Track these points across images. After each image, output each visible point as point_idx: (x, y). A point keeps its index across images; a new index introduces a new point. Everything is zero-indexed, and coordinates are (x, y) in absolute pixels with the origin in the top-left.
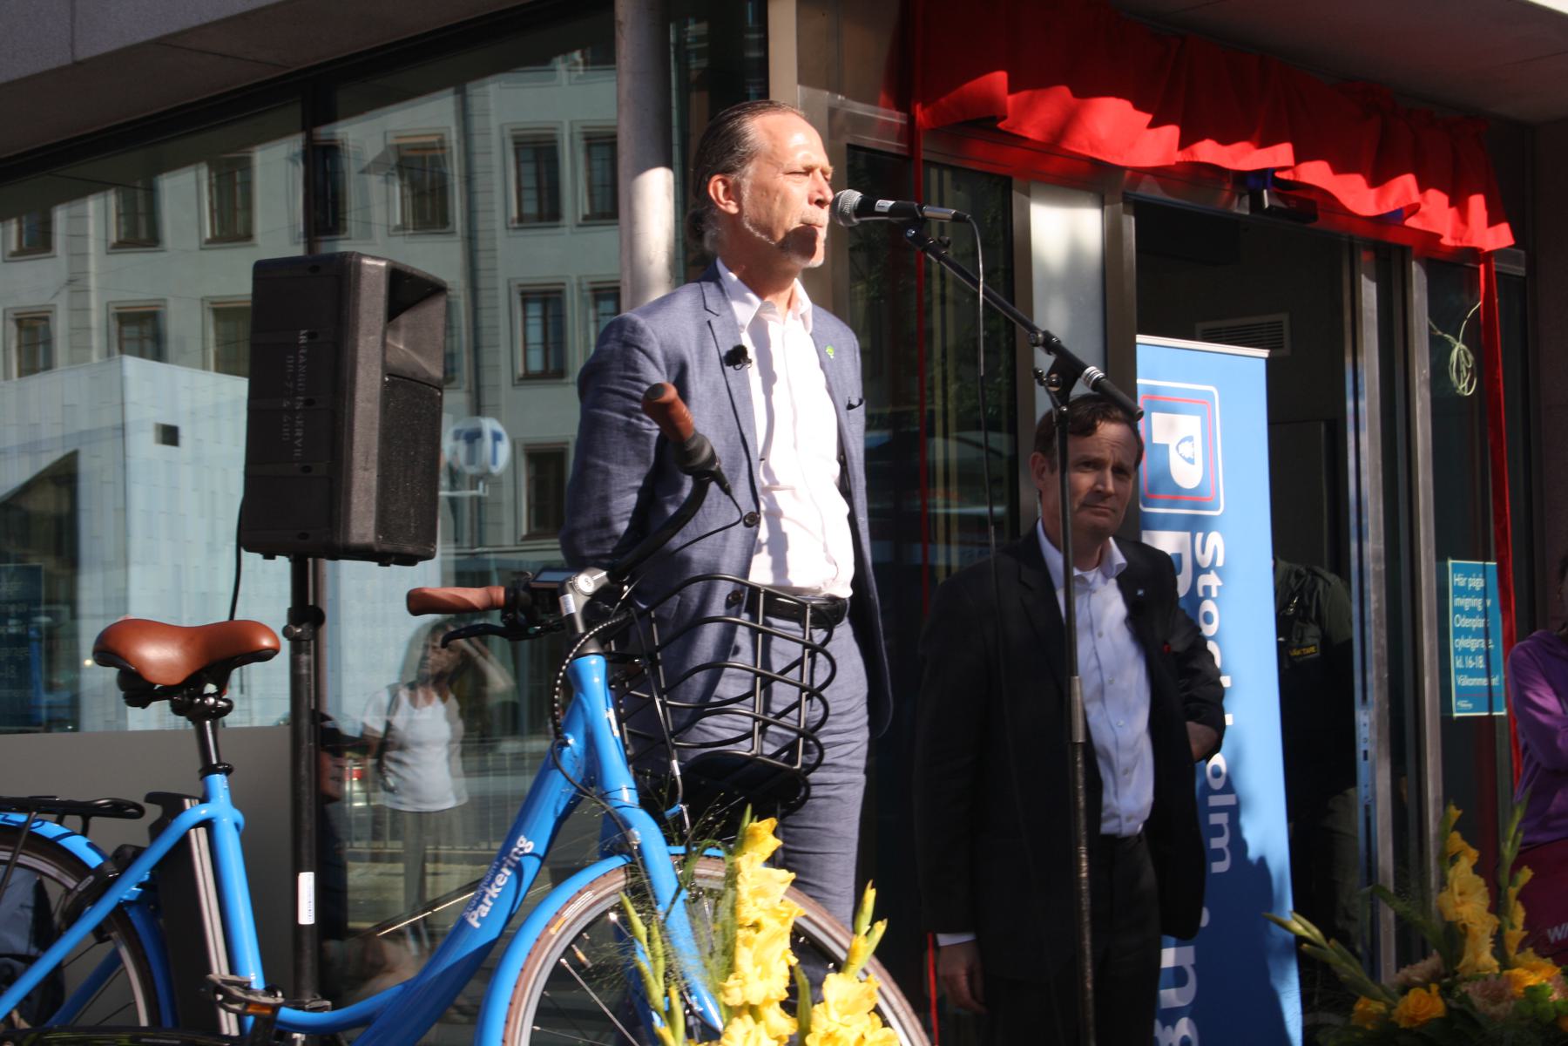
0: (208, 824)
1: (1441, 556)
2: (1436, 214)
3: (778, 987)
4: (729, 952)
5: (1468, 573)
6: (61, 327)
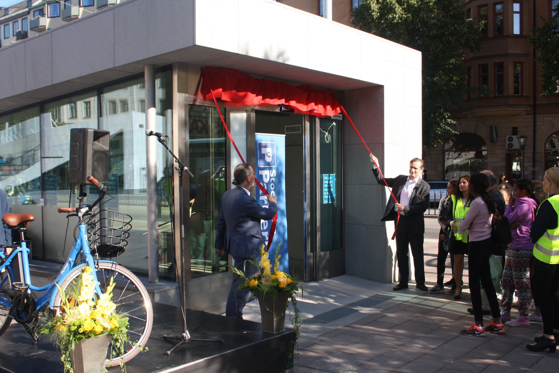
0: (21, 252)
1: (322, 172)
2: (319, 109)
3: (92, 295)
4: (80, 291)
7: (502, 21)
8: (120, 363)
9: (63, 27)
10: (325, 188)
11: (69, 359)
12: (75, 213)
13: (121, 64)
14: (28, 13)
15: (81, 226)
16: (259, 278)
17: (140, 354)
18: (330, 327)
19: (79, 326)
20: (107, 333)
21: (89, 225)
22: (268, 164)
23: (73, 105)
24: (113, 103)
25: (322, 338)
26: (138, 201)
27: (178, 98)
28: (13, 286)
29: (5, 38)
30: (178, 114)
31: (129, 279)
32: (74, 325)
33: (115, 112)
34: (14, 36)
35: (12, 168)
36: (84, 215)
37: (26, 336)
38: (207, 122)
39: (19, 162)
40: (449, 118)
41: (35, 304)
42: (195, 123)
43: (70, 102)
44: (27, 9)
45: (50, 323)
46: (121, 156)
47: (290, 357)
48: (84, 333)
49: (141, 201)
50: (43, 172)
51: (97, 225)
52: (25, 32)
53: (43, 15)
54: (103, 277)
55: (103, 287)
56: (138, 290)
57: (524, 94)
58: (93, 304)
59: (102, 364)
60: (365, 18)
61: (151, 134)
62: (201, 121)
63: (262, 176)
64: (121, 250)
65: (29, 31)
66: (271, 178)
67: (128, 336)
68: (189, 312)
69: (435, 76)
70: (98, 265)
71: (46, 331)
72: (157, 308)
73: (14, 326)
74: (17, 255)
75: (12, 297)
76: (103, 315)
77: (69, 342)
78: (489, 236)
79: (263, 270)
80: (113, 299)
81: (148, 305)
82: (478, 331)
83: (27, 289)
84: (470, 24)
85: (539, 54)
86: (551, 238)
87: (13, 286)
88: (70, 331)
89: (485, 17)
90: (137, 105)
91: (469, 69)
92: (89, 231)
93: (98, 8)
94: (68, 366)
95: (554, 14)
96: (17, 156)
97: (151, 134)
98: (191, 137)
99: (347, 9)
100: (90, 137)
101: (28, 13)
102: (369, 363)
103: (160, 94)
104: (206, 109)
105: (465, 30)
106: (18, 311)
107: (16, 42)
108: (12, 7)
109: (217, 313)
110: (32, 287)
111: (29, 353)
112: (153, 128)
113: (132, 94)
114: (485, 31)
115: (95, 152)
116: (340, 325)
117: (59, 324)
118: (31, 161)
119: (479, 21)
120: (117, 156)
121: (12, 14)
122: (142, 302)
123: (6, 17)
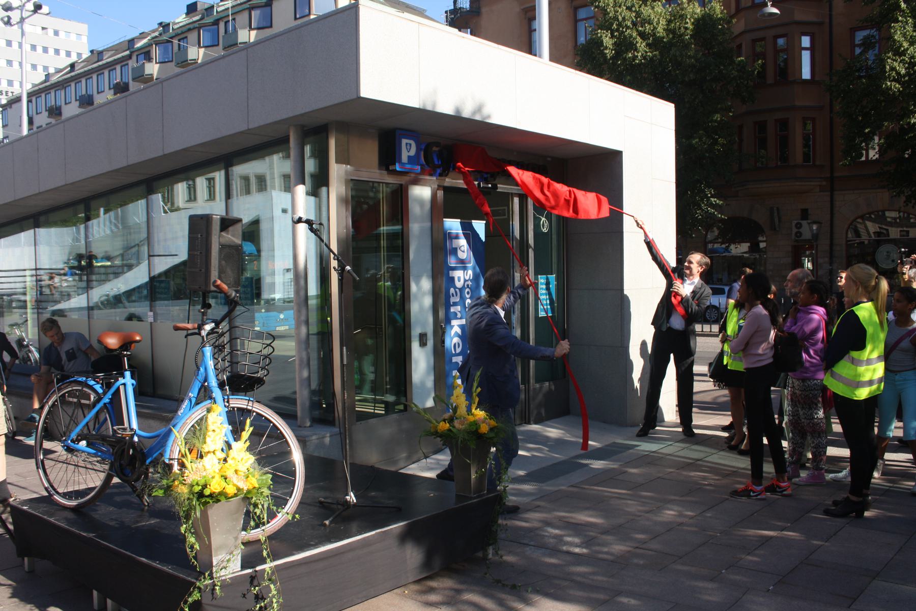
0: (124, 384)
3: (221, 444)
4: (205, 438)
6: (268, 178)
7: (785, 61)
8: (261, 537)
10: (455, 304)
12: (197, 331)
14: (130, 57)
17: (288, 525)
19: (205, 486)
20: (242, 496)
21: (215, 347)
22: (462, 262)
23: (191, 182)
24: (246, 179)
25: (538, 503)
27: (337, 171)
29: (98, 93)
31: (271, 422)
32: (197, 484)
33: (248, 192)
36: (208, 334)
37: (133, 500)
40: (712, 196)
41: (144, 456)
43: (187, 179)
44: (128, 53)
45: (165, 482)
48: (211, 496)
50: (152, 275)
54: (236, 419)
55: (237, 433)
56: (284, 437)
57: (818, 163)
58: (223, 455)
59: (236, 538)
61: (300, 220)
63: (453, 279)
64: (260, 381)
66: (465, 281)
68: (353, 466)
70: (228, 402)
71: (160, 493)
73: (117, 486)
74: (118, 389)
75: (113, 447)
76: (236, 471)
78: (771, 360)
79: (455, 409)
80: (249, 449)
81: (297, 456)
83: (132, 436)
85: (837, 107)
86: (856, 362)
88: (191, 492)
89: (763, 55)
90: (278, 181)
92: (216, 356)
93: (224, 48)
94: (192, 539)
95: (858, 51)
97: (300, 220)
99: (570, 46)
100: (216, 226)
101: (130, 57)
102: (604, 537)
103: (310, 166)
104: (373, 187)
106: (121, 465)
108: (107, 50)
109: (393, 469)
111: (138, 522)
112: (301, 213)
113: (271, 167)
114: (762, 74)
115: (223, 247)
117: (176, 483)
121: (107, 59)
122: (289, 453)
123: (100, 63)
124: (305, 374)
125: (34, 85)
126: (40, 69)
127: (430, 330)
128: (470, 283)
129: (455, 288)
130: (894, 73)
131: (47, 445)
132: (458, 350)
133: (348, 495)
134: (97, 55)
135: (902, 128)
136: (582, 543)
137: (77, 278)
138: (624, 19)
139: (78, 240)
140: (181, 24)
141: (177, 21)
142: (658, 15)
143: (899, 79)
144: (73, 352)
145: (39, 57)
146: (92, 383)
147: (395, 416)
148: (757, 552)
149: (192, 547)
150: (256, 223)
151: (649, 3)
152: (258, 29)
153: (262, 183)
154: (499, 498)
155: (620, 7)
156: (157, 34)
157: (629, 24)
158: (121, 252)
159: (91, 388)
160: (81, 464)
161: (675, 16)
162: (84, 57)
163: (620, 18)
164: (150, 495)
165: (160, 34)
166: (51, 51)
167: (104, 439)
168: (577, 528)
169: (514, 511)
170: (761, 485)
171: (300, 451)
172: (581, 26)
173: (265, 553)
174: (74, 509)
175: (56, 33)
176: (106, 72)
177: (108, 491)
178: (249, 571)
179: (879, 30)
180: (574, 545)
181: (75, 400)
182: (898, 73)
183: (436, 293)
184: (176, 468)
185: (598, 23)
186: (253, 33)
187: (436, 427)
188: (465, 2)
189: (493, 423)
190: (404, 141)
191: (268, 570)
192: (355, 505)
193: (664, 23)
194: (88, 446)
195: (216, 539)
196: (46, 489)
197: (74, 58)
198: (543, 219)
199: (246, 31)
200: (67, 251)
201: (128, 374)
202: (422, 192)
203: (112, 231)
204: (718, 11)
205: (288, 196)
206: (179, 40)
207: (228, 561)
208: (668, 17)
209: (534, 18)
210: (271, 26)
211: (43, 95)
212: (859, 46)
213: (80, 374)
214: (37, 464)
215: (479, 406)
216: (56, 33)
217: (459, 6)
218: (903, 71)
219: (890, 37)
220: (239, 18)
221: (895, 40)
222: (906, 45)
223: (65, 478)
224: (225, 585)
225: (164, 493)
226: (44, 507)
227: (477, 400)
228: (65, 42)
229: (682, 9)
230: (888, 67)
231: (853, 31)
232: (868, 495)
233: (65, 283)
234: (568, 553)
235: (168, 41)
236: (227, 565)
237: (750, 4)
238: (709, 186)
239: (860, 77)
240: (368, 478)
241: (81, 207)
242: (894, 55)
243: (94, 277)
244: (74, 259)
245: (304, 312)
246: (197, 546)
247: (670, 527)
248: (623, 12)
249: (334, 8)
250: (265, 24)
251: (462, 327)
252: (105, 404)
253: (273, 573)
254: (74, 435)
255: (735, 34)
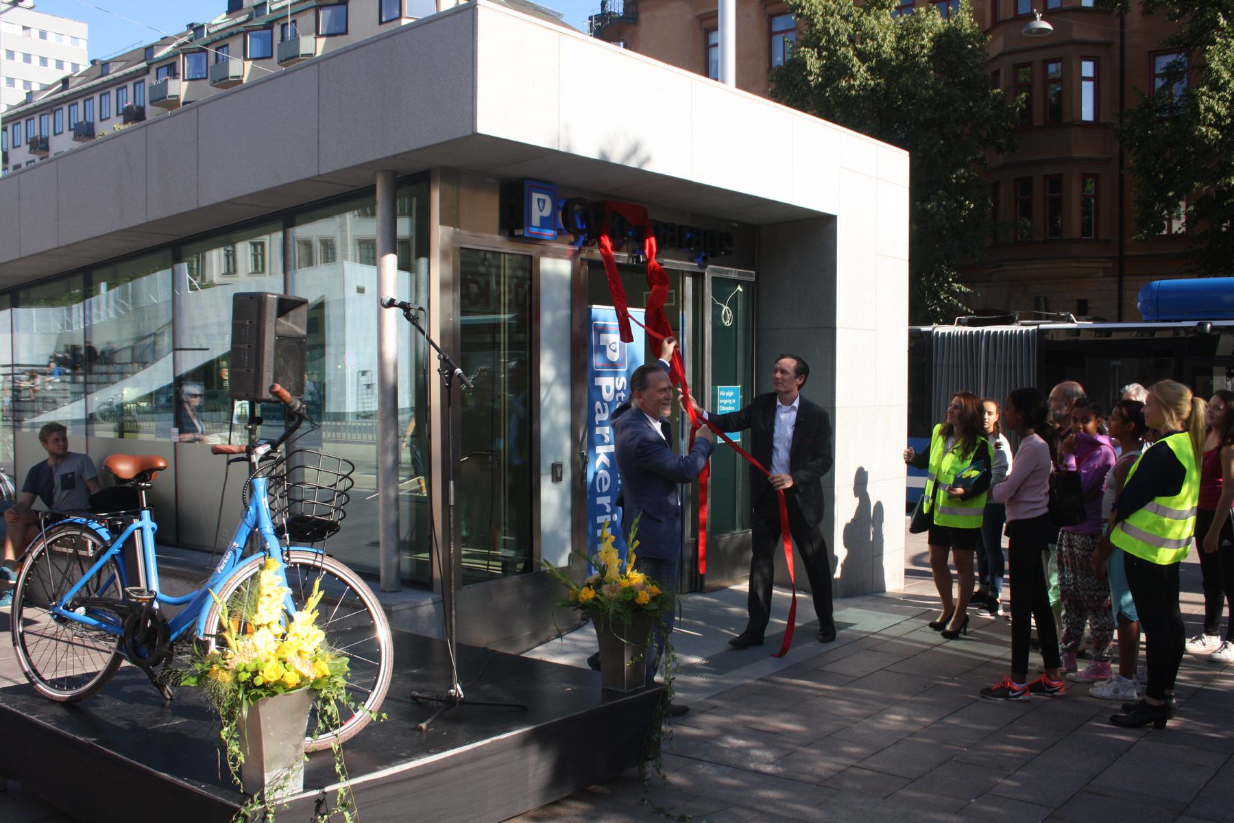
0: (141, 529)
1: (717, 381)
3: (278, 615)
4: (256, 606)
5: (726, 391)
7: (1059, 95)
8: (332, 745)
9: (77, 151)
10: (602, 424)
11: (235, 736)
12: (244, 455)
13: (330, 170)
14: (147, 71)
15: (256, 480)
16: (598, 585)
17: (370, 728)
18: (728, 680)
19: (256, 673)
20: (308, 687)
21: (271, 479)
22: (613, 365)
23: (230, 248)
24: (308, 244)
25: (715, 702)
26: (364, 436)
27: (440, 234)
28: (126, 595)
29: (101, 120)
30: (437, 270)
31: (347, 584)
32: (245, 670)
33: (310, 262)
34: (118, 115)
35: (111, 369)
36: (261, 460)
37: (149, 691)
38: (488, 283)
39: (126, 357)
40: (954, 281)
41: (167, 629)
42: (472, 282)
43: (225, 244)
44: (144, 64)
45: (198, 666)
46: (321, 347)
47: (654, 738)
48: (264, 686)
49: (359, 436)
50: (178, 374)
51: (285, 479)
52: (139, 107)
53: (174, 75)
54: (299, 581)
55: (300, 599)
56: (365, 605)
57: (1102, 237)
58: (281, 630)
59: (298, 747)
60: (796, 86)
61: (391, 303)
62: (476, 282)
63: (599, 388)
64: (333, 527)
65: (148, 106)
66: (616, 391)
67: (347, 694)
68: (463, 650)
69: (928, 200)
70: (288, 555)
71: (192, 682)
72: (398, 640)
73: (128, 671)
74: (133, 534)
75: (124, 617)
76: (299, 653)
77: (236, 704)
78: (1046, 510)
79: (603, 570)
80: (318, 622)
81: (383, 634)
82: (1014, 691)
83: (151, 601)
84: (999, 103)
85: (1130, 160)
86: (1164, 512)
87: (126, 595)
88: (237, 681)
89: (1028, 87)
90: (351, 249)
91: (996, 185)
92: (272, 491)
93: (280, 62)
94: (234, 748)
95: (1159, 83)
96: (125, 345)
97: (391, 303)
98: (463, 314)
99: (762, 69)
100: (271, 309)
101: (147, 71)
102: (806, 750)
103: (404, 227)
104: (485, 259)
105: (989, 111)
106: (134, 642)
107: (122, 127)
108: (115, 60)
109: (512, 652)
110: (160, 596)
111: (157, 722)
112: (390, 293)
113: (343, 228)
114: (1027, 113)
115: (281, 339)
116: (748, 678)
117: (215, 667)
118: (149, 357)
119: (1016, 94)
120: (314, 347)
121: (115, 73)
122: (372, 628)
123: (105, 79)
124: (392, 516)
125: (11, 108)
126: (19, 84)
127: (565, 456)
128: (623, 395)
129: (602, 401)
130: (1210, 116)
131: (28, 613)
132: (605, 488)
133: (450, 690)
134: (101, 66)
135: (1220, 192)
136: (778, 759)
137: (68, 378)
138: (837, 32)
139: (70, 326)
140: (220, 27)
141: (214, 22)
142: (884, 28)
143: (1218, 123)
144: (73, 478)
145: (17, 68)
146: (95, 525)
147: (515, 578)
148: (1018, 773)
149: (235, 759)
150: (321, 306)
151: (872, 12)
152: (328, 35)
153: (329, 251)
154: (663, 693)
155: (832, 15)
156: (185, 39)
157: (844, 39)
158: (130, 343)
159: (94, 533)
160: (76, 640)
161: (907, 30)
162: (82, 69)
163: (832, 32)
164: (175, 684)
165: (191, 40)
166: (35, 61)
167: (111, 605)
168: (769, 738)
169: (682, 713)
170: (1022, 681)
171: (387, 625)
172: (778, 41)
173: (338, 768)
174: (67, 704)
175: (43, 35)
176: (113, 92)
177: (115, 678)
178: (315, 792)
179: (1188, 55)
180: (763, 759)
181: (71, 551)
182: (1217, 115)
183: (575, 407)
184: (213, 648)
185: (802, 37)
186: (321, 42)
187: (577, 594)
188: (617, 5)
189: (655, 590)
190: (536, 196)
191: (341, 791)
192: (462, 702)
193: (893, 39)
194: (87, 614)
195: (270, 747)
196: (26, 674)
197: (67, 71)
198: (726, 308)
199: (311, 38)
200: (54, 342)
201: (146, 514)
202: (557, 267)
203: (117, 313)
204: (966, 24)
205: (370, 271)
206: (217, 49)
207: (286, 778)
208: (899, 32)
209: (715, 28)
210: (346, 33)
211: (23, 122)
212: (1160, 76)
213: (78, 512)
214: (14, 639)
215: (637, 567)
216: (43, 35)
217: (609, 9)
218: (1223, 112)
219: (1205, 66)
220: (301, 20)
221: (1211, 69)
222: (1226, 75)
223: (53, 660)
224: (280, 812)
225: (198, 682)
226: (22, 700)
227: (634, 557)
228: (64, 48)
229: (918, 21)
230: (1202, 107)
231: (1153, 55)
232: (1171, 697)
233: (52, 384)
234: (757, 772)
235: (201, 50)
236: (285, 783)
237: (1011, 16)
238: (949, 267)
239: (1162, 120)
240: (484, 665)
241: (79, 279)
242: (1211, 90)
243: (94, 378)
244: (67, 351)
245: (392, 434)
246: (241, 758)
247: (897, 738)
248: (836, 24)
249: (434, 12)
250: (337, 30)
251: (609, 455)
252: (113, 556)
253: (349, 795)
254: (67, 599)
255: (991, 56)
